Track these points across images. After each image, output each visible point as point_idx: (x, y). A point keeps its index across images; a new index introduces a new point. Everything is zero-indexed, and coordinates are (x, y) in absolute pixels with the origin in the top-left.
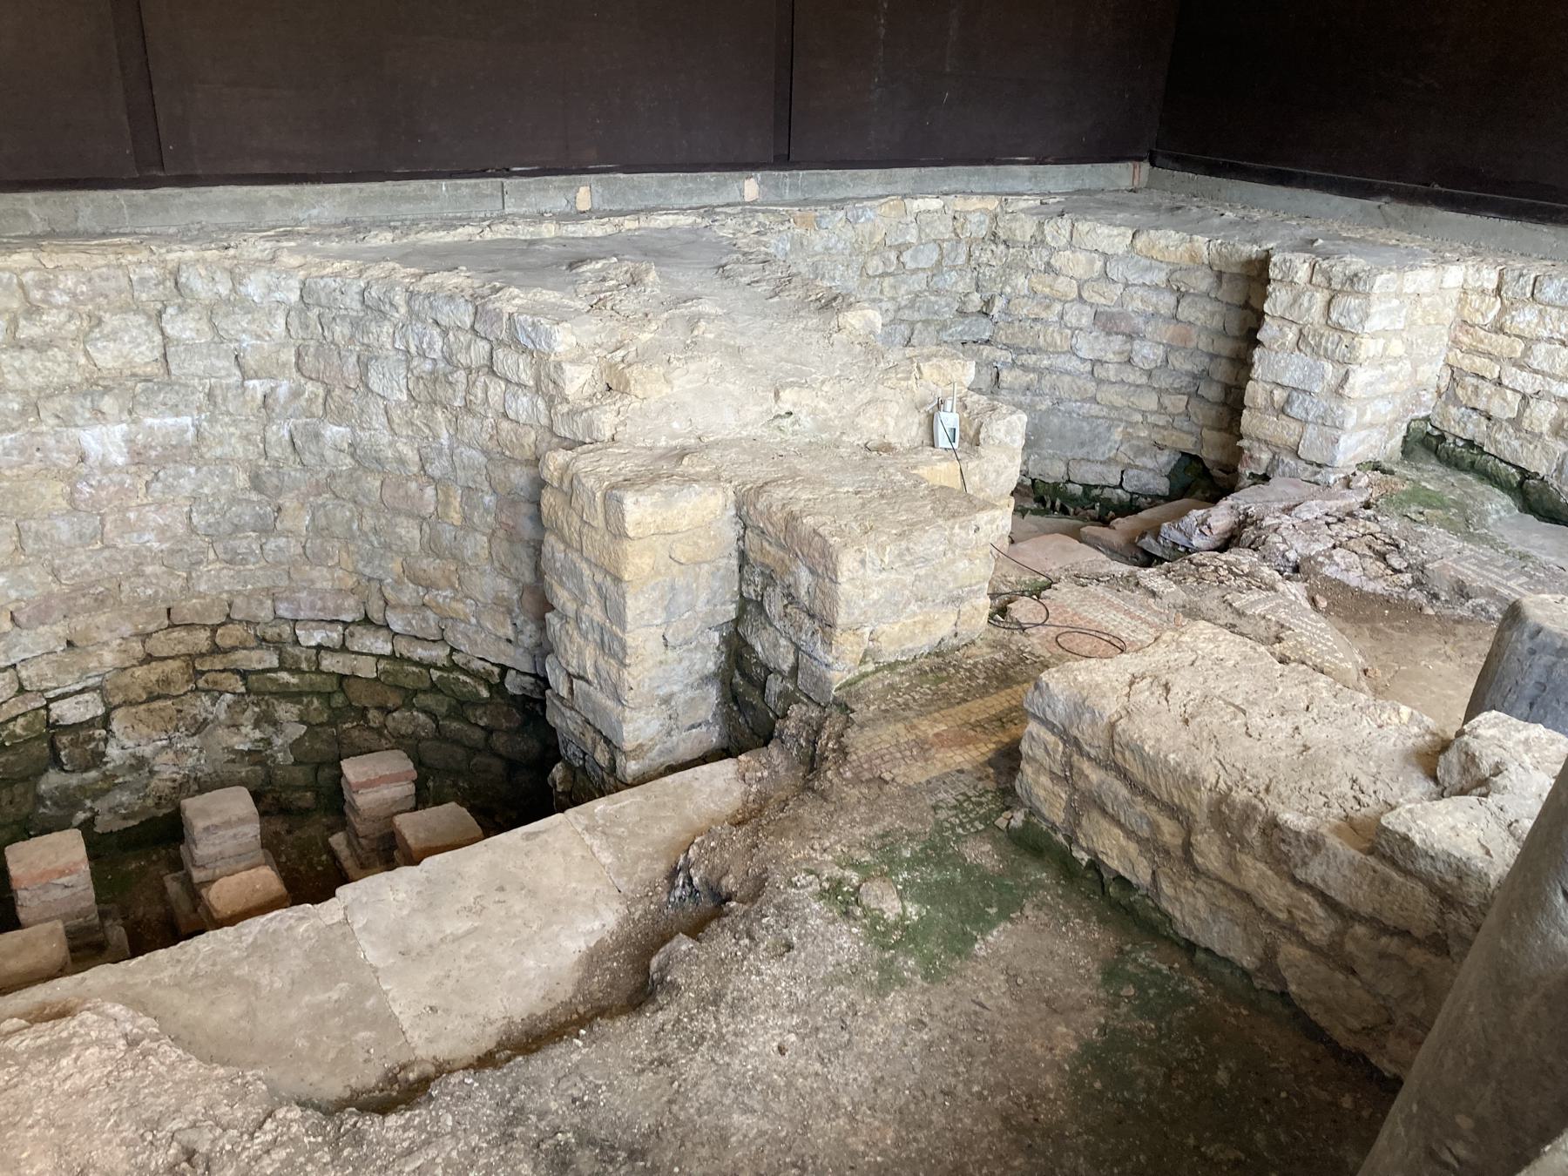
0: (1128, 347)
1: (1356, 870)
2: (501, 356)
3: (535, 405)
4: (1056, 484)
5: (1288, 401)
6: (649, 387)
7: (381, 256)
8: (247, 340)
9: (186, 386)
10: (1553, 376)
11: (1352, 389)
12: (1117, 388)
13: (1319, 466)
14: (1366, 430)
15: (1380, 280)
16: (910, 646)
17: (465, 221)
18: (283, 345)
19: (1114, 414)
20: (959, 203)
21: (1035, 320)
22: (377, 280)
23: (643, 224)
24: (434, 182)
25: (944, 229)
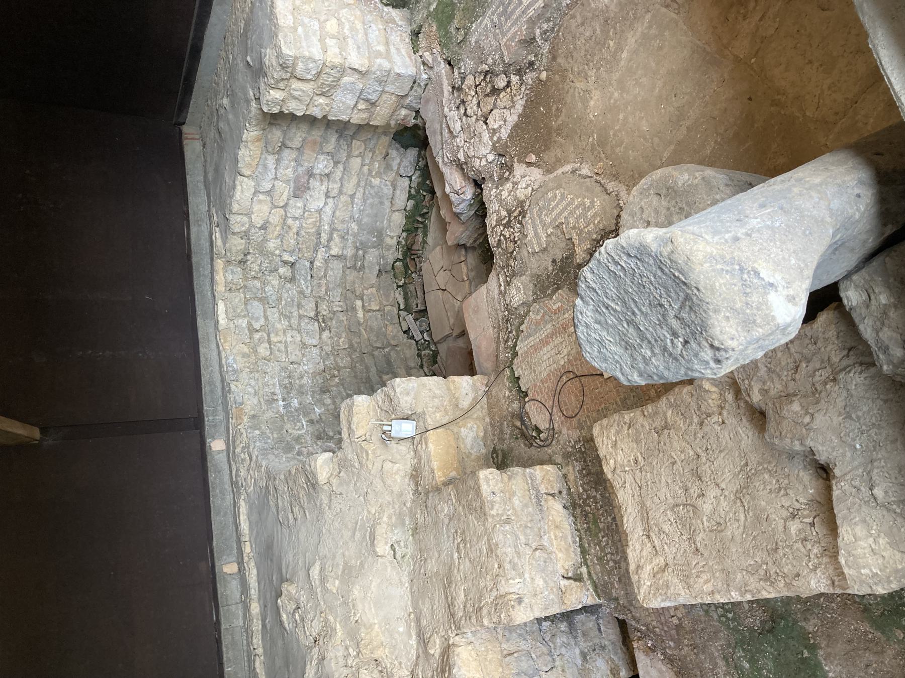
0: (318, 176)
4: (407, 217)
5: (367, 100)
12: (345, 183)
13: (414, 82)
16: (570, 537)
19: (363, 183)
20: (220, 288)
21: (298, 234)
23: (247, 539)
25: (238, 298)
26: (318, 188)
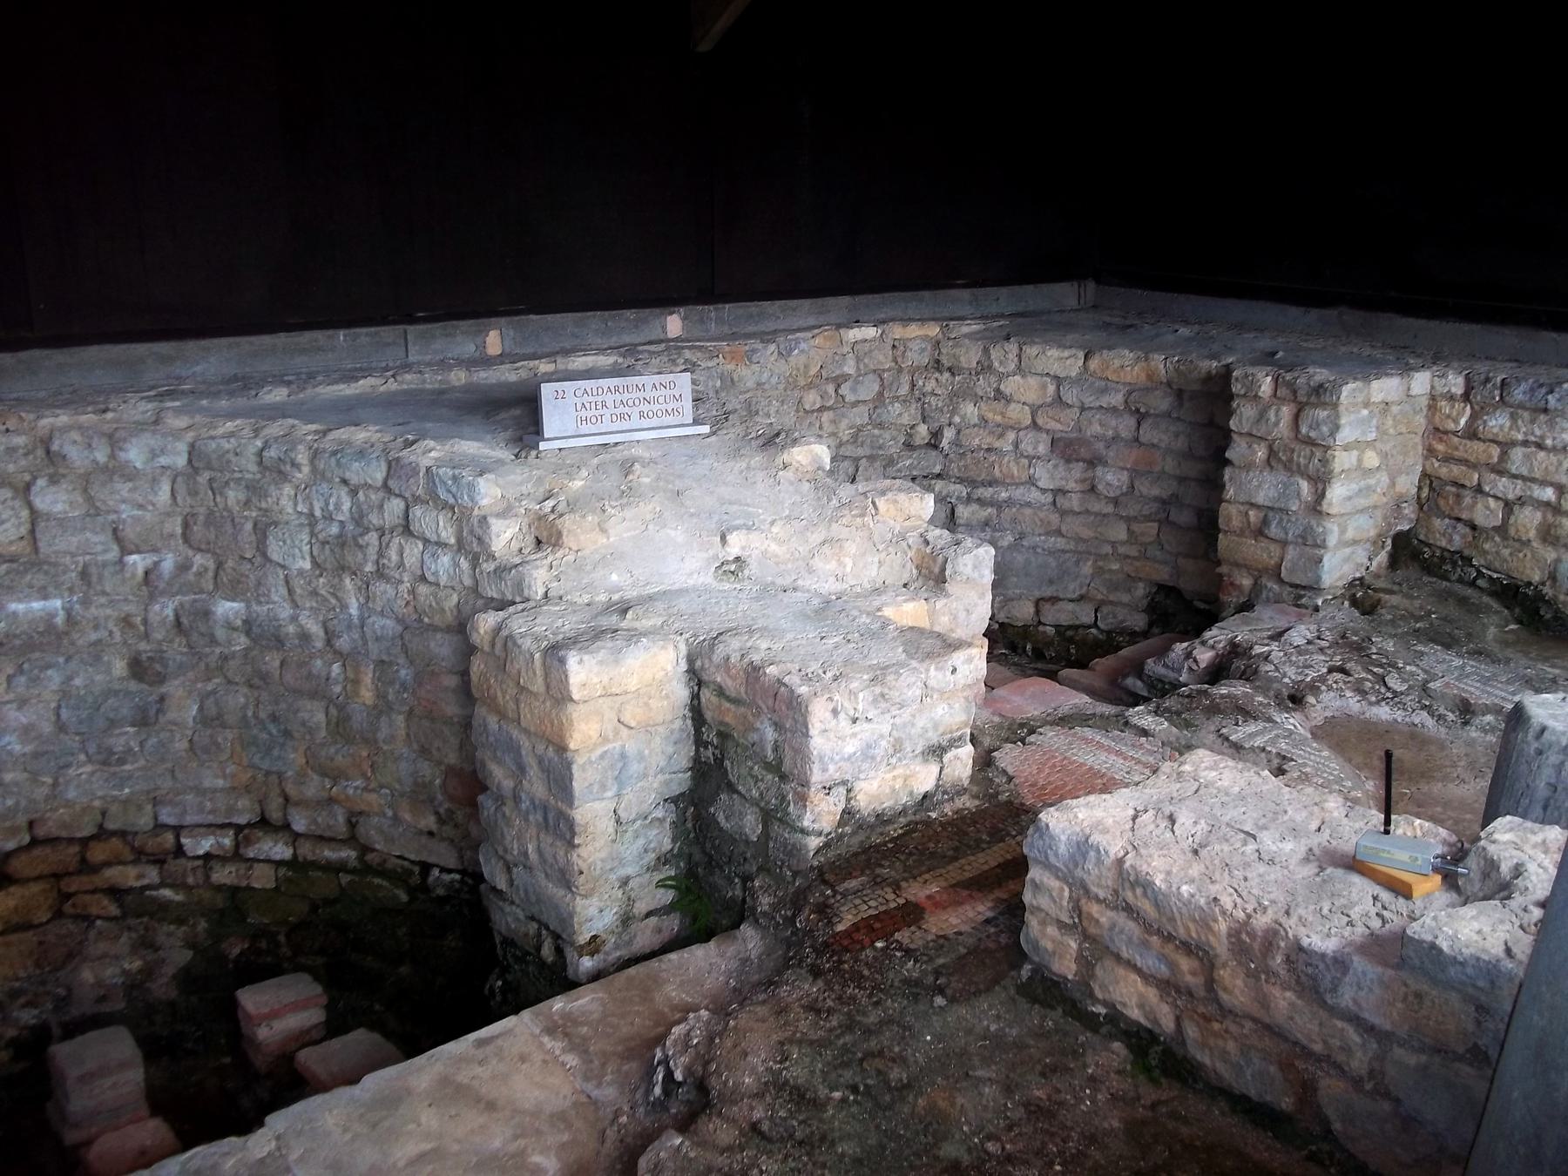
1: (1387, 987)
2: (418, 513)
3: (456, 565)
5: (1265, 522)
6: (581, 535)
7: (277, 412)
8: (127, 512)
9: (55, 565)
10: (1533, 480)
11: (1330, 504)
12: (1081, 518)
14: (1347, 550)
15: (1346, 390)
17: (366, 372)
18: (168, 514)
20: (897, 331)
21: (988, 450)
22: (276, 439)
23: (561, 367)
24: (330, 332)
25: (883, 359)
26: (1071, 477)
